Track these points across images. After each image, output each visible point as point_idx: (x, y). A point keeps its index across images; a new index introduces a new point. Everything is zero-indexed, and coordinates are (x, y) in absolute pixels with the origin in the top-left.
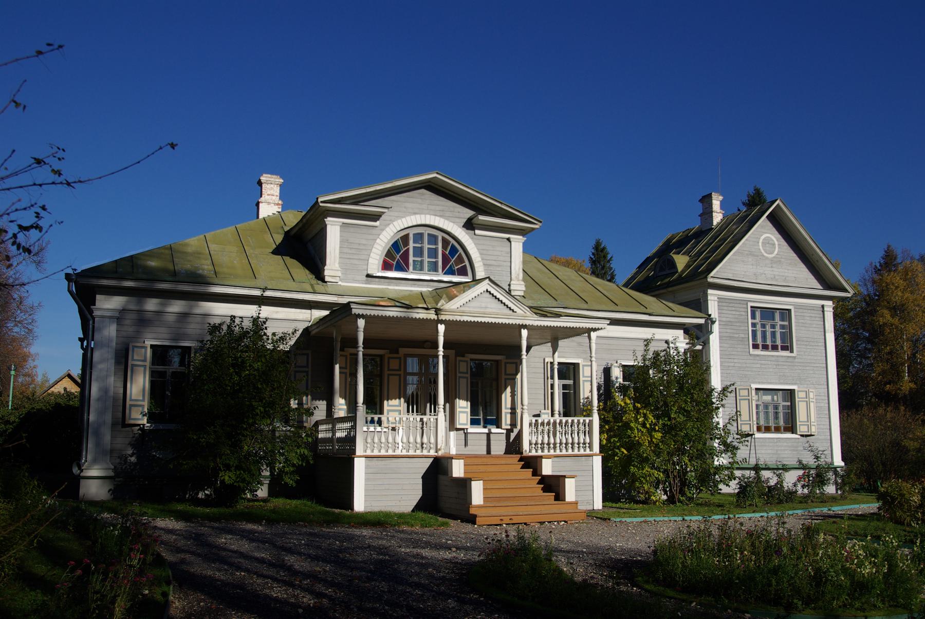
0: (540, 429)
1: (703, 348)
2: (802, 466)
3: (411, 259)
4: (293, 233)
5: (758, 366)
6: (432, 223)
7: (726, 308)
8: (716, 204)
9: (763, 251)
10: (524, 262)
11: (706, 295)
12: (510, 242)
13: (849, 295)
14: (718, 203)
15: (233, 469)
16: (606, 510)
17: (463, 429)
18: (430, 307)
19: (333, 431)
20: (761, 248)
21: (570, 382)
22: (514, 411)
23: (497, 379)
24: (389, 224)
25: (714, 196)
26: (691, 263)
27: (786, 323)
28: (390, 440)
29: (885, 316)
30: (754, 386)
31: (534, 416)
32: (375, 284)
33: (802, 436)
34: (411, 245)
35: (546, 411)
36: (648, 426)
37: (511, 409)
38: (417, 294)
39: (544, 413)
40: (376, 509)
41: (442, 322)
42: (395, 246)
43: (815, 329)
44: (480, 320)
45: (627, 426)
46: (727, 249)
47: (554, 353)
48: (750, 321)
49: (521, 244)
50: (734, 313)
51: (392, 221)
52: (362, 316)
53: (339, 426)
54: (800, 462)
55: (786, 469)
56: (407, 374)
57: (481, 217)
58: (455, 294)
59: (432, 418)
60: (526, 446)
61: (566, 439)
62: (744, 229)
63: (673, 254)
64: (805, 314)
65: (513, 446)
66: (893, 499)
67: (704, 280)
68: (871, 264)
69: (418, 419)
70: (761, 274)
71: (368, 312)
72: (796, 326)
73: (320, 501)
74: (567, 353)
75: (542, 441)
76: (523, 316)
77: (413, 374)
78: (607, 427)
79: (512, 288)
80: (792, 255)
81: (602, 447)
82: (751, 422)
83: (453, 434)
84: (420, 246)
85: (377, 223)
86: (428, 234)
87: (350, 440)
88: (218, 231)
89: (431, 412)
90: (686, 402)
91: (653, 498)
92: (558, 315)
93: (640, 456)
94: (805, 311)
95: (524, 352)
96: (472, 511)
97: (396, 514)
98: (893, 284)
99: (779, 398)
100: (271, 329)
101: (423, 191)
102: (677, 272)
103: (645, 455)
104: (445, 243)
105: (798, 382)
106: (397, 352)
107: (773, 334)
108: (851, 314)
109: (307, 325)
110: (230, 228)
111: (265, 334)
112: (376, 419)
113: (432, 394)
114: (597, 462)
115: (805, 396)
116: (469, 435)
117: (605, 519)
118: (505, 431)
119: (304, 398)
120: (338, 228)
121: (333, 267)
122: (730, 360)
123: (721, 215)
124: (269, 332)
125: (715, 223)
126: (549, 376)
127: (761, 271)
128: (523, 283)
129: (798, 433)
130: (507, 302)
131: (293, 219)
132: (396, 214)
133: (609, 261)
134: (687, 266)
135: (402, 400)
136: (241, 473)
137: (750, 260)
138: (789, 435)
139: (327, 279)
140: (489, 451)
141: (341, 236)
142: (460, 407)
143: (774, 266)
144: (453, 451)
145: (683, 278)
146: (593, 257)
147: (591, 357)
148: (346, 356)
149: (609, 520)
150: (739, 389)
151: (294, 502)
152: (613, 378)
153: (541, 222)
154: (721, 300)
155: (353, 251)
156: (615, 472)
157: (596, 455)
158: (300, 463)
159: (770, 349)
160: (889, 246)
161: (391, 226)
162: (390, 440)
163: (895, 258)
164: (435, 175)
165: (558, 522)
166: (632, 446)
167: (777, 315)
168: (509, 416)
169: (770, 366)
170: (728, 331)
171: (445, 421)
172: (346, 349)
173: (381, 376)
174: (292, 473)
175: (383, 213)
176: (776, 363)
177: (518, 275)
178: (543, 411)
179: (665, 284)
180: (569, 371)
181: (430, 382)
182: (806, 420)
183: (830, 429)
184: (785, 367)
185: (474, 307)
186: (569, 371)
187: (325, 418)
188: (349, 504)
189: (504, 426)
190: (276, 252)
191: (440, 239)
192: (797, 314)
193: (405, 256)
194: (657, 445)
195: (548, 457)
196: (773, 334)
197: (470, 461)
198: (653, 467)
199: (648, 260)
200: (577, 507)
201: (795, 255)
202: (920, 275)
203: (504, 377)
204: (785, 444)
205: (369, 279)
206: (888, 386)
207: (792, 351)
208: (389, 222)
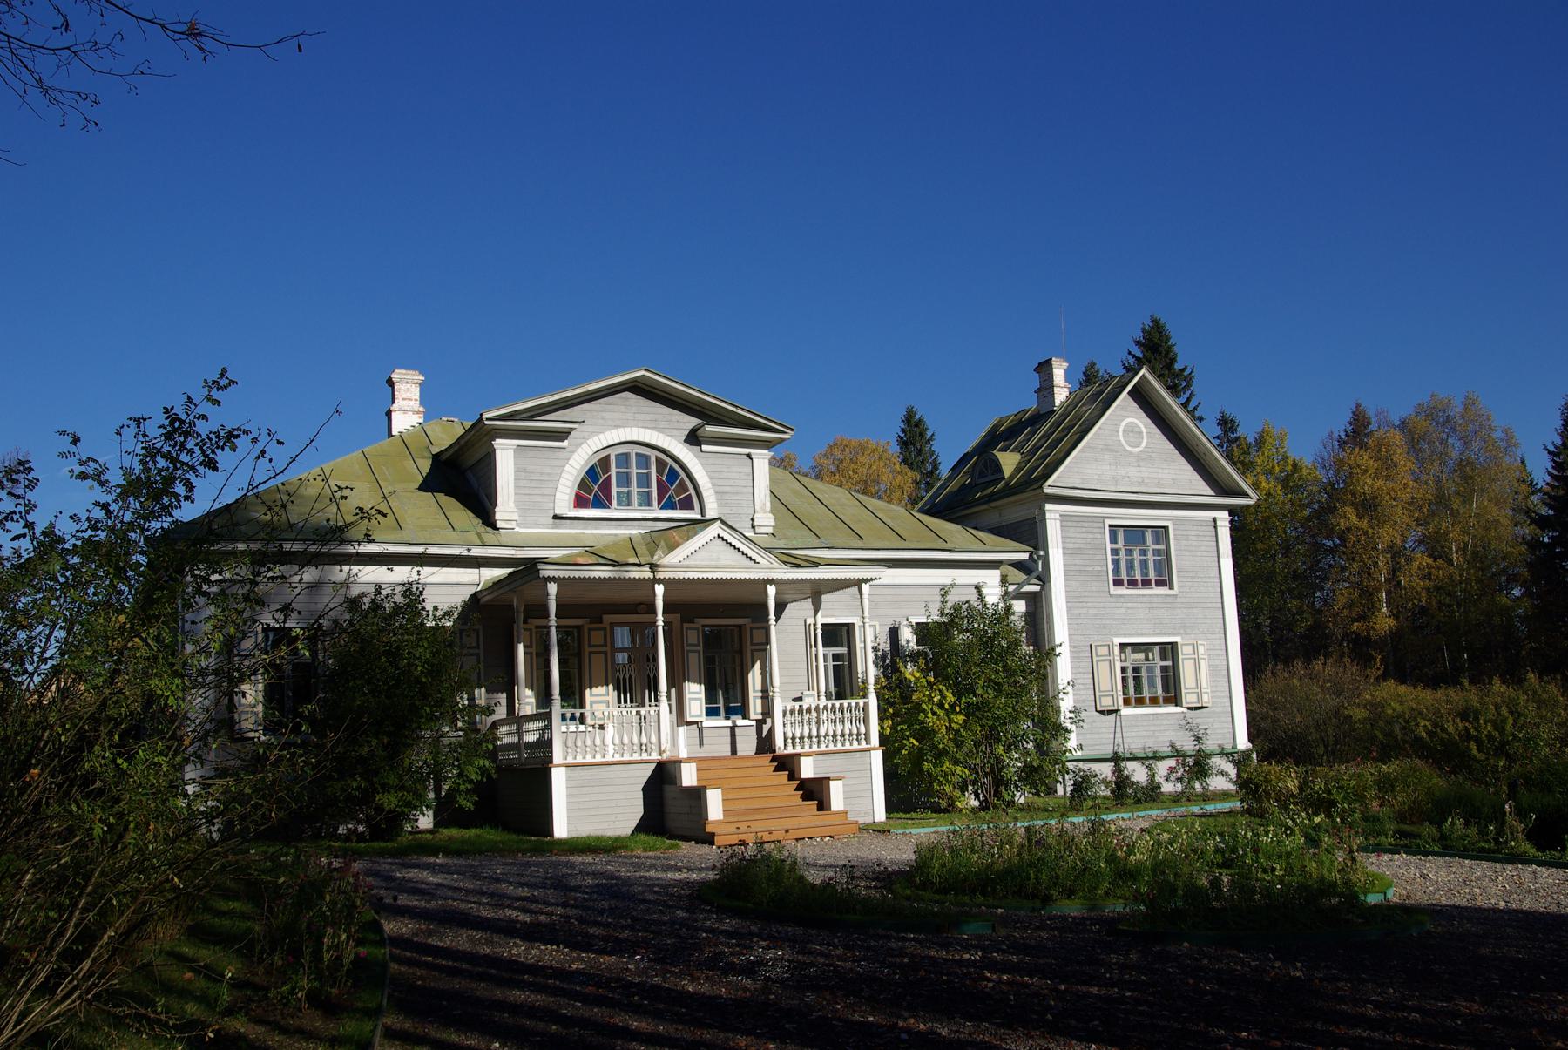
0: (806, 716)
1: (1042, 589)
2: (1178, 754)
3: (614, 490)
4: (444, 457)
5: (1123, 610)
6: (641, 439)
7: (1072, 530)
8: (1059, 374)
9: (1125, 444)
10: (772, 480)
11: (1043, 512)
12: (751, 459)
13: (1251, 502)
14: (1062, 372)
15: (392, 791)
16: (891, 822)
17: (697, 723)
18: (643, 563)
19: (520, 733)
20: (1121, 439)
21: (843, 650)
22: (766, 694)
23: (741, 652)
24: (582, 443)
25: (1055, 362)
26: (1022, 465)
27: (1162, 547)
28: (598, 742)
29: (1348, 517)
30: (1117, 641)
31: (795, 700)
32: (566, 528)
33: (1189, 708)
34: (614, 470)
35: (811, 692)
36: (947, 706)
37: (762, 691)
38: (624, 540)
39: (808, 696)
40: (584, 834)
41: (660, 581)
42: (592, 473)
43: (1205, 554)
44: (710, 576)
45: (918, 708)
46: (1070, 445)
47: (816, 614)
48: (1109, 546)
49: (767, 461)
50: (1085, 535)
51: (585, 439)
52: (553, 579)
53: (526, 726)
54: (1173, 746)
55: (1158, 757)
56: (615, 650)
57: (709, 428)
58: (676, 542)
59: (653, 710)
60: (779, 742)
61: (858, 729)
62: (1097, 412)
63: (999, 451)
64: (1189, 533)
65: (765, 744)
66: (1257, 786)
67: (1040, 491)
68: (1331, 434)
69: (634, 711)
70: (1123, 477)
71: (561, 574)
72: (1176, 550)
73: (507, 828)
74: (835, 610)
75: (842, 731)
76: (769, 568)
77: (622, 650)
78: (891, 710)
79: (756, 523)
80: (1167, 447)
81: (884, 740)
82: (1114, 693)
83: (682, 730)
84: (625, 470)
85: (565, 444)
86: (637, 454)
87: (545, 745)
88: (339, 460)
89: (650, 701)
90: (997, 672)
91: (958, 803)
92: (815, 564)
93: (934, 747)
94: (1187, 528)
95: (772, 616)
96: (709, 829)
97: (610, 838)
98: (1359, 466)
99: (1156, 654)
100: (431, 600)
101: (627, 394)
102: (1003, 478)
103: (941, 746)
104: (661, 464)
105: (1182, 631)
106: (601, 622)
107: (1144, 564)
108: (1306, 513)
109: (473, 589)
110: (354, 454)
111: (424, 609)
112: (578, 715)
113: (652, 677)
114: (877, 758)
115: (1191, 652)
116: (704, 731)
117: (884, 832)
118: (754, 723)
119: (477, 692)
120: (511, 453)
121: (506, 508)
122: (1080, 605)
123: (1066, 390)
124: (429, 606)
125: (1057, 403)
126: (813, 643)
127: (1123, 473)
128: (771, 515)
129: (1184, 705)
130: (746, 551)
131: (445, 435)
132: (590, 429)
133: (928, 442)
134: (1018, 469)
135: (611, 687)
136: (403, 795)
137: (1106, 457)
138: (1171, 709)
139: (499, 525)
140: (734, 751)
141: (515, 464)
142: (690, 693)
143: (1141, 464)
144: (684, 754)
145: (1011, 488)
146: (903, 435)
147: (863, 618)
148: (530, 630)
149: (889, 832)
150: (1096, 646)
151: (473, 832)
152: (903, 642)
153: (793, 430)
154: (1064, 517)
155: (533, 485)
156: (903, 770)
157: (875, 749)
158: (479, 778)
159: (1140, 586)
160: (1358, 406)
161: (584, 446)
162: (598, 742)
163: (1369, 423)
164: (643, 373)
165: (822, 837)
166: (925, 734)
167: (1149, 535)
168: (759, 702)
169: (1140, 611)
170: (1077, 562)
171: (670, 712)
172: (529, 620)
173: (579, 655)
174: (468, 791)
175: (573, 429)
176: (1149, 605)
177: (764, 504)
178: (806, 693)
179: (986, 496)
180: (837, 635)
181: (648, 660)
182: (1194, 686)
183: (1231, 698)
184: (1163, 611)
185: (702, 559)
186: (837, 635)
187: (505, 716)
188: (550, 832)
189: (752, 716)
190: (426, 486)
191: (653, 459)
192: (1177, 532)
193: (606, 487)
194: (957, 732)
195: (808, 755)
196: (1144, 564)
197: (704, 765)
198: (956, 762)
199: (965, 459)
200: (846, 818)
201: (1172, 447)
202: (1399, 451)
203: (749, 647)
205: (558, 521)
206: (1356, 624)
207: (1171, 588)
208: (580, 441)
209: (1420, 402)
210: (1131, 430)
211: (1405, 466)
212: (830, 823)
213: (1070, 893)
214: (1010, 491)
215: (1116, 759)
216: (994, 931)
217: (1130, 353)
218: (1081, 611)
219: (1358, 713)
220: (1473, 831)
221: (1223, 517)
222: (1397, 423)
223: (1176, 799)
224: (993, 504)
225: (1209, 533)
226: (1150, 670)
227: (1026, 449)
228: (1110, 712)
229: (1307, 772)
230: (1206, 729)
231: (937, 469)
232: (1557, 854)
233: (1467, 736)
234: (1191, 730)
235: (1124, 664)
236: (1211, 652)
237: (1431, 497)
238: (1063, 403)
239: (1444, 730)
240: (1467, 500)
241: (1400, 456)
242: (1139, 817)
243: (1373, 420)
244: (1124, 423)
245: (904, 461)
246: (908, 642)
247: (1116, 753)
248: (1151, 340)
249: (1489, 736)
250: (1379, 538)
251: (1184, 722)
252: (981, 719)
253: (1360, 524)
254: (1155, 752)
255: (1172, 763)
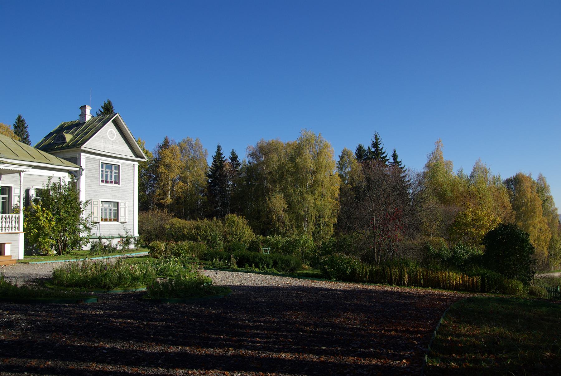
1: (77, 181)
2: (121, 237)
5: (103, 190)
7: (89, 162)
9: (109, 137)
26: (73, 139)
27: (117, 171)
29: (162, 169)
33: (121, 223)
36: (49, 219)
43: (130, 175)
45: (38, 218)
48: (101, 169)
50: (93, 165)
55: (113, 238)
62: (101, 125)
64: (126, 168)
66: (154, 248)
72: (121, 173)
75: (5, 226)
81: (25, 229)
93: (44, 233)
94: (126, 166)
98: (166, 155)
102: (66, 142)
103: (47, 232)
107: (111, 176)
108: (148, 166)
114: (22, 236)
115: (97, 204)
122: (90, 187)
123: (90, 117)
125: (87, 120)
127: (107, 146)
129: (120, 222)
133: (26, 128)
134: (72, 140)
138: (115, 223)
143: (114, 144)
145: (69, 146)
146: (16, 124)
147: (20, 185)
149: (28, 263)
150: (94, 201)
152: (31, 195)
154: (87, 158)
157: (21, 233)
160: (166, 137)
163: (169, 142)
166: (40, 228)
170: (90, 173)
182: (97, 215)
192: (122, 167)
194: (53, 228)
196: (111, 176)
199: (51, 134)
200: (11, 258)
201: (123, 140)
202: (178, 151)
204: (113, 227)
206: (161, 200)
207: (119, 184)
209: (184, 138)
210: (111, 133)
211: (179, 156)
212: (4, 260)
213: (116, 285)
214: (68, 147)
215: (100, 238)
216: (98, 301)
217: (99, 110)
218: (90, 189)
219: (167, 227)
220: (221, 263)
221: (137, 164)
222: (177, 143)
223: (120, 251)
224: (62, 151)
225: (132, 169)
226: (110, 210)
227: (75, 134)
228: (96, 223)
229: (166, 244)
230: (130, 230)
231: (28, 137)
232: (244, 269)
233: (198, 234)
234: (125, 230)
235: (102, 208)
236: (129, 206)
237: (185, 166)
238: (89, 121)
239: (191, 232)
240: (193, 168)
241: (178, 153)
242: (113, 258)
243: (170, 142)
244: (109, 130)
245: (15, 133)
246: (33, 195)
247: (100, 236)
248: (107, 107)
249: (203, 234)
250: (170, 176)
251: (123, 227)
252: (62, 224)
253: (165, 171)
254: (112, 236)
255: (119, 240)
